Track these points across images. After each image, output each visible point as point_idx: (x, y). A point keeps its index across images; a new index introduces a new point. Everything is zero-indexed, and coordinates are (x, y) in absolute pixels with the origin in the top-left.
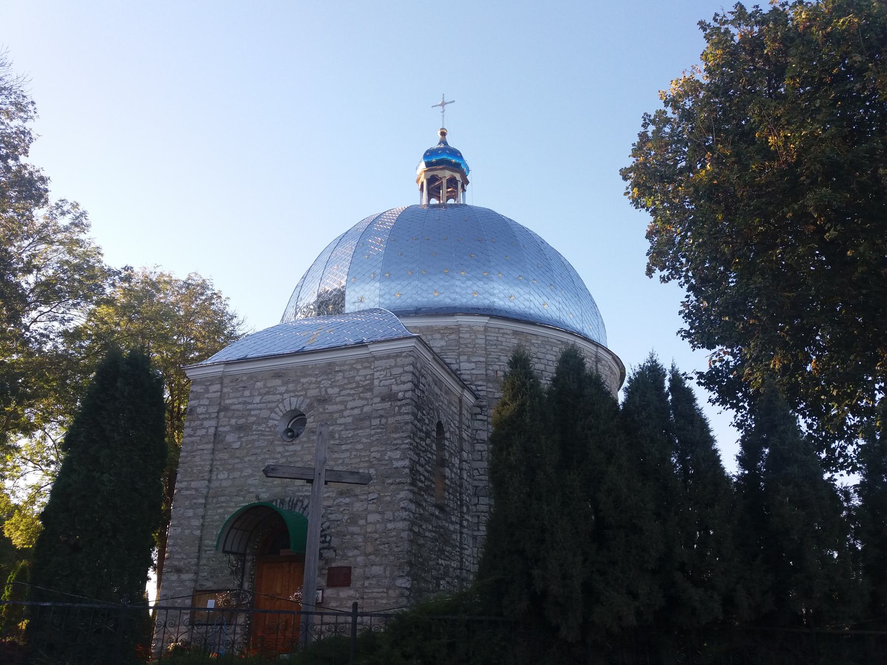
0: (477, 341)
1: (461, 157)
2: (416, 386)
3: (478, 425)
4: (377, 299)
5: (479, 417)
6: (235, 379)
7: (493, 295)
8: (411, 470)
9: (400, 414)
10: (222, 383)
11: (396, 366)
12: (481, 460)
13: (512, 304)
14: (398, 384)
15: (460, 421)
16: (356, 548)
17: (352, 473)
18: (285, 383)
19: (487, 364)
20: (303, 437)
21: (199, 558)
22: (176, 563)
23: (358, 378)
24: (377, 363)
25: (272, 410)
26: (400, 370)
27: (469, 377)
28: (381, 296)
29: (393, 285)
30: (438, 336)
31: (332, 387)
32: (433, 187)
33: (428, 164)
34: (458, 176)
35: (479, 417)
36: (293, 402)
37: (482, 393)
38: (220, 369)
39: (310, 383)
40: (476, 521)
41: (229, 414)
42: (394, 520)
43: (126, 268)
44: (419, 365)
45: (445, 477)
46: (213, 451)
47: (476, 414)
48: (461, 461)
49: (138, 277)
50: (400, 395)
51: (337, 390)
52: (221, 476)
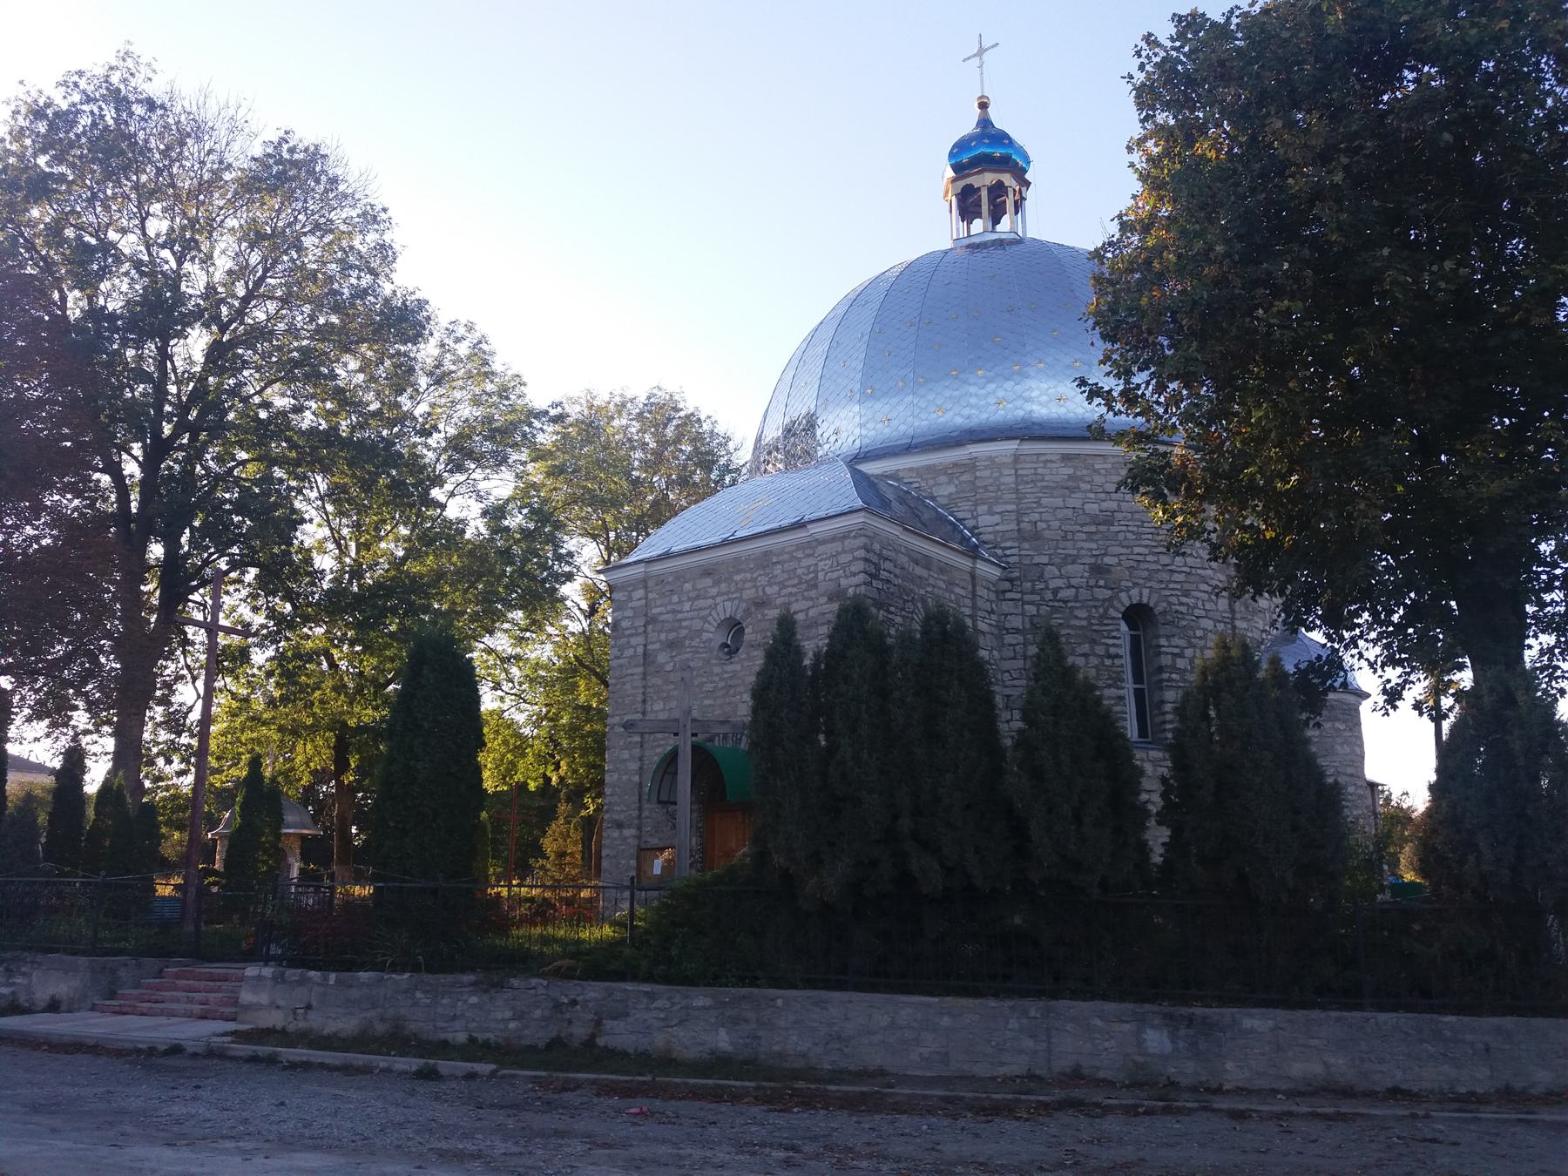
0: (1003, 480)
1: (1011, 142)
2: (874, 576)
3: (1007, 607)
4: (857, 431)
5: (1009, 595)
6: (661, 581)
7: (1028, 400)
10: (646, 587)
11: (844, 551)
12: (1014, 658)
13: (1062, 411)
14: (846, 577)
15: (974, 607)
17: (722, 722)
18: (716, 583)
19: (1020, 514)
20: (742, 653)
21: (640, 809)
22: (616, 817)
23: (799, 571)
24: (821, 549)
25: (705, 619)
26: (849, 557)
27: (992, 537)
28: (861, 426)
29: (878, 405)
30: (943, 479)
31: (770, 584)
32: (967, 206)
33: (957, 168)
34: (1008, 179)
35: (1009, 595)
36: (726, 609)
37: (1012, 560)
38: (641, 569)
39: (744, 581)
41: (659, 627)
43: (555, 405)
44: (877, 547)
46: (644, 676)
47: (1004, 592)
49: (574, 411)
51: (776, 588)
52: (656, 707)
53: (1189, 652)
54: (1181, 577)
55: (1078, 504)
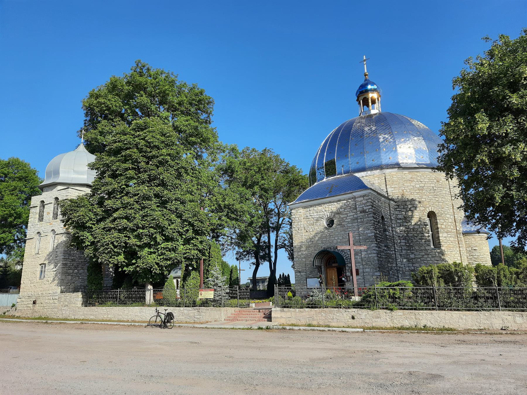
2: (372, 206)
8: (375, 236)
9: (368, 217)
15: (390, 213)
16: (359, 263)
40: (400, 248)
42: (371, 254)
45: (387, 235)
48: (392, 228)
50: (367, 210)
53: (445, 224)
54: (441, 204)
55: (414, 185)
